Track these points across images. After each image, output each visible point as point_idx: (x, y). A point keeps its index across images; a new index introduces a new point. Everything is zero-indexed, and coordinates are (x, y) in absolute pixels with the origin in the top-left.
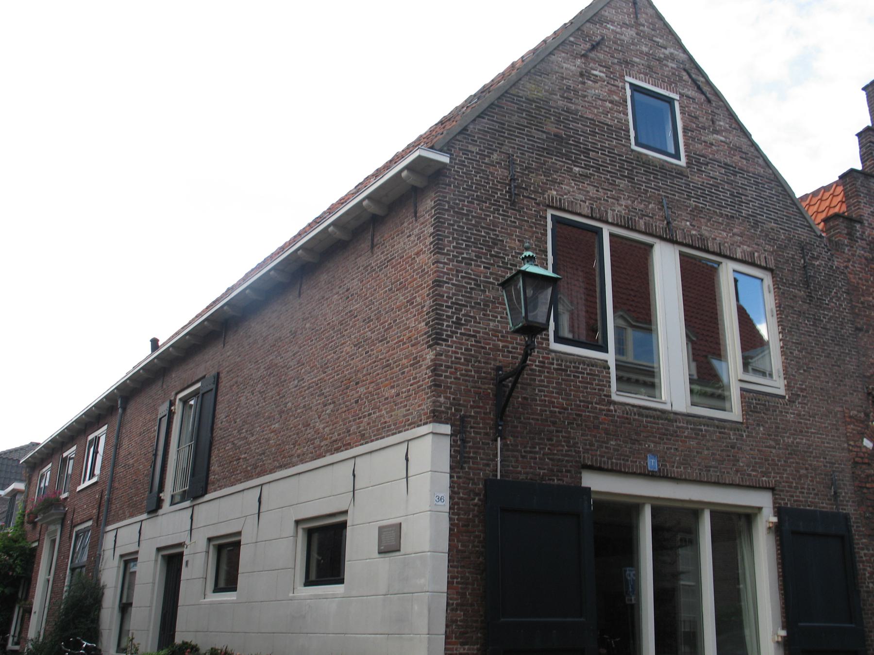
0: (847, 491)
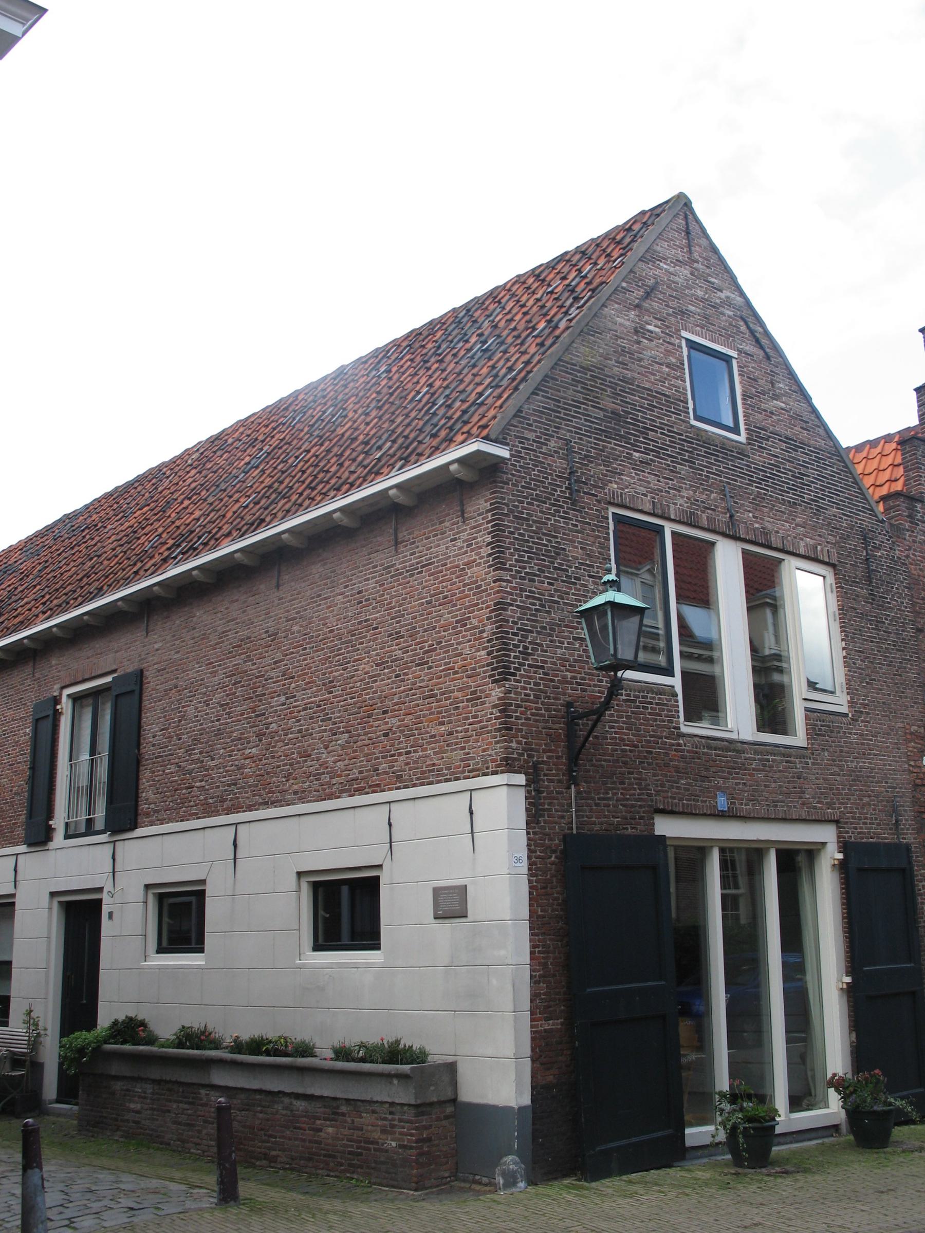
0: (907, 818)
